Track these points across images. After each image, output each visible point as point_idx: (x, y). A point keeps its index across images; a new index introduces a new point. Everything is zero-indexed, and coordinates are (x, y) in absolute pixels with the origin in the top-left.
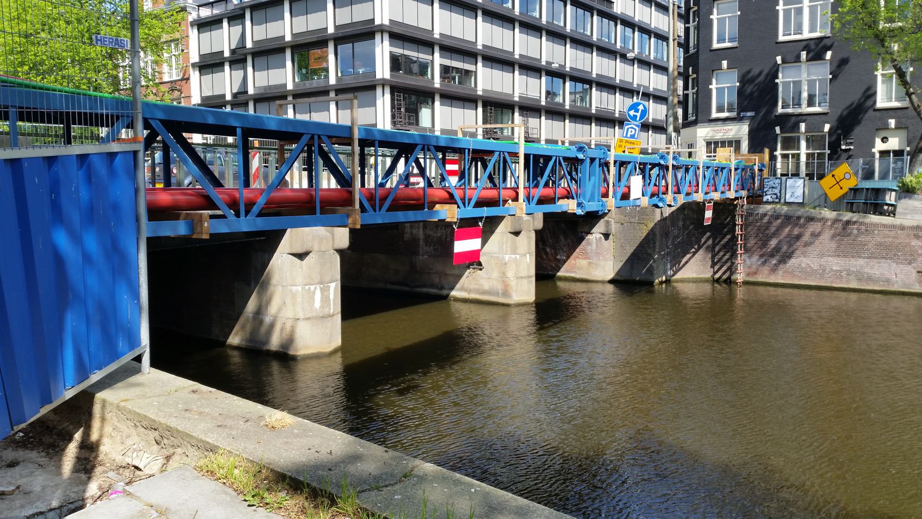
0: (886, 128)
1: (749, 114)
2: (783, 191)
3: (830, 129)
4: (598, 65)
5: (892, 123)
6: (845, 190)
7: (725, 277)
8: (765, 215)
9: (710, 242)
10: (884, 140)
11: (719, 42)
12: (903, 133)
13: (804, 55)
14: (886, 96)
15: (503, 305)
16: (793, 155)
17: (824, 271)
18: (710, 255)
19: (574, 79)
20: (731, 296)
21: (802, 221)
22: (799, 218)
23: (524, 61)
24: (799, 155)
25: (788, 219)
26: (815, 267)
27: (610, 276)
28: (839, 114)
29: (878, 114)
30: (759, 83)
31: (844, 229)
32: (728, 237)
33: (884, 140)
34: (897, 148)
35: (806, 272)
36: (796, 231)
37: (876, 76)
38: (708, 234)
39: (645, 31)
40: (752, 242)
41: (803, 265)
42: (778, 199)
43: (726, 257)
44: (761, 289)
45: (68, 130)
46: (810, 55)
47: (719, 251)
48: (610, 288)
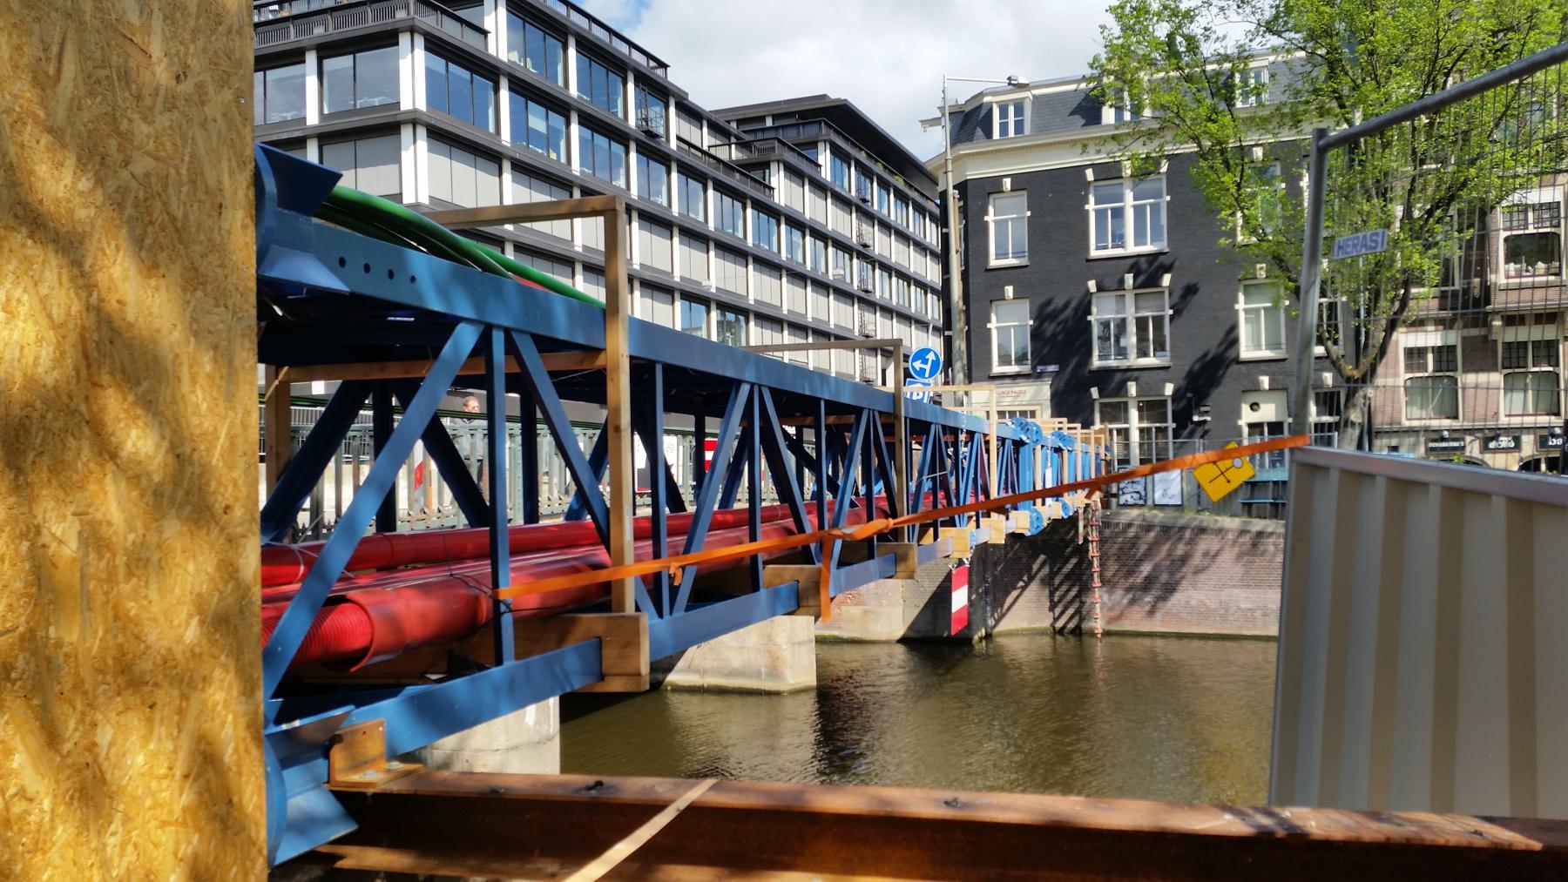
0: (1256, 389)
1: (1052, 368)
2: (1149, 487)
3: (1176, 392)
4: (754, 286)
5: (1265, 381)
6: (1235, 484)
7: (1071, 625)
8: (1130, 525)
9: (1046, 570)
10: (1254, 406)
11: (998, 257)
12: (1281, 397)
13: (1129, 279)
14: (1252, 344)
15: (769, 693)
16: (1119, 431)
17: (1226, 610)
18: (1047, 592)
19: (724, 307)
20: (1084, 658)
21: (1188, 534)
22: (1183, 528)
23: (648, 276)
24: (1127, 431)
25: (1166, 530)
26: (1212, 604)
27: (900, 632)
28: (1187, 368)
29: (1243, 368)
30: (1066, 321)
31: (1254, 545)
32: (1074, 561)
33: (1254, 406)
34: (1273, 419)
35: (1199, 613)
36: (1180, 550)
37: (1237, 312)
38: (1042, 557)
39: (820, 235)
40: (1112, 568)
41: (1193, 603)
42: (1143, 501)
43: (1073, 593)
44: (1129, 642)
45: (700, 426)
46: (1141, 278)
47: (1061, 584)
48: (900, 650)
